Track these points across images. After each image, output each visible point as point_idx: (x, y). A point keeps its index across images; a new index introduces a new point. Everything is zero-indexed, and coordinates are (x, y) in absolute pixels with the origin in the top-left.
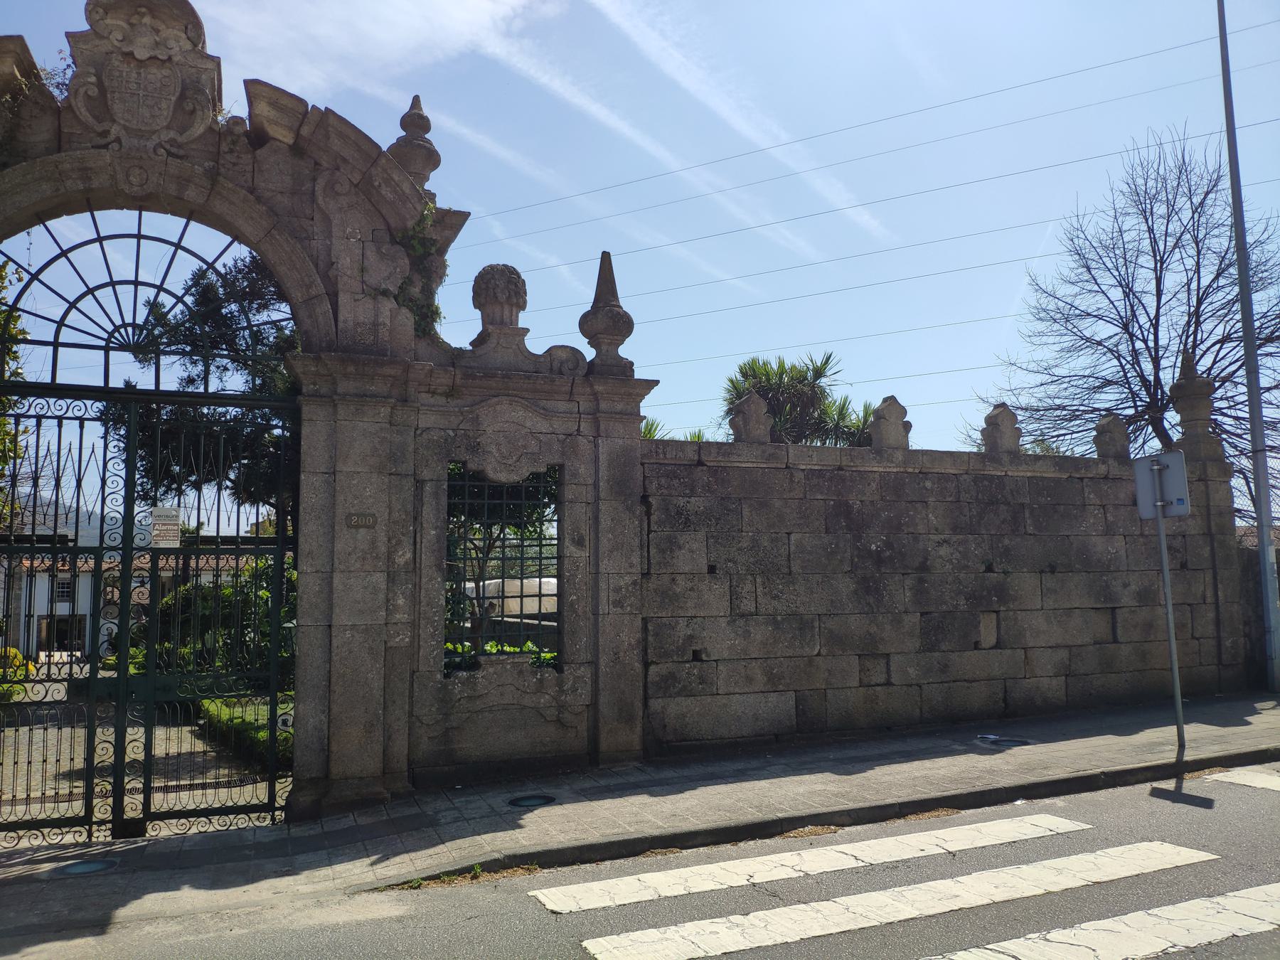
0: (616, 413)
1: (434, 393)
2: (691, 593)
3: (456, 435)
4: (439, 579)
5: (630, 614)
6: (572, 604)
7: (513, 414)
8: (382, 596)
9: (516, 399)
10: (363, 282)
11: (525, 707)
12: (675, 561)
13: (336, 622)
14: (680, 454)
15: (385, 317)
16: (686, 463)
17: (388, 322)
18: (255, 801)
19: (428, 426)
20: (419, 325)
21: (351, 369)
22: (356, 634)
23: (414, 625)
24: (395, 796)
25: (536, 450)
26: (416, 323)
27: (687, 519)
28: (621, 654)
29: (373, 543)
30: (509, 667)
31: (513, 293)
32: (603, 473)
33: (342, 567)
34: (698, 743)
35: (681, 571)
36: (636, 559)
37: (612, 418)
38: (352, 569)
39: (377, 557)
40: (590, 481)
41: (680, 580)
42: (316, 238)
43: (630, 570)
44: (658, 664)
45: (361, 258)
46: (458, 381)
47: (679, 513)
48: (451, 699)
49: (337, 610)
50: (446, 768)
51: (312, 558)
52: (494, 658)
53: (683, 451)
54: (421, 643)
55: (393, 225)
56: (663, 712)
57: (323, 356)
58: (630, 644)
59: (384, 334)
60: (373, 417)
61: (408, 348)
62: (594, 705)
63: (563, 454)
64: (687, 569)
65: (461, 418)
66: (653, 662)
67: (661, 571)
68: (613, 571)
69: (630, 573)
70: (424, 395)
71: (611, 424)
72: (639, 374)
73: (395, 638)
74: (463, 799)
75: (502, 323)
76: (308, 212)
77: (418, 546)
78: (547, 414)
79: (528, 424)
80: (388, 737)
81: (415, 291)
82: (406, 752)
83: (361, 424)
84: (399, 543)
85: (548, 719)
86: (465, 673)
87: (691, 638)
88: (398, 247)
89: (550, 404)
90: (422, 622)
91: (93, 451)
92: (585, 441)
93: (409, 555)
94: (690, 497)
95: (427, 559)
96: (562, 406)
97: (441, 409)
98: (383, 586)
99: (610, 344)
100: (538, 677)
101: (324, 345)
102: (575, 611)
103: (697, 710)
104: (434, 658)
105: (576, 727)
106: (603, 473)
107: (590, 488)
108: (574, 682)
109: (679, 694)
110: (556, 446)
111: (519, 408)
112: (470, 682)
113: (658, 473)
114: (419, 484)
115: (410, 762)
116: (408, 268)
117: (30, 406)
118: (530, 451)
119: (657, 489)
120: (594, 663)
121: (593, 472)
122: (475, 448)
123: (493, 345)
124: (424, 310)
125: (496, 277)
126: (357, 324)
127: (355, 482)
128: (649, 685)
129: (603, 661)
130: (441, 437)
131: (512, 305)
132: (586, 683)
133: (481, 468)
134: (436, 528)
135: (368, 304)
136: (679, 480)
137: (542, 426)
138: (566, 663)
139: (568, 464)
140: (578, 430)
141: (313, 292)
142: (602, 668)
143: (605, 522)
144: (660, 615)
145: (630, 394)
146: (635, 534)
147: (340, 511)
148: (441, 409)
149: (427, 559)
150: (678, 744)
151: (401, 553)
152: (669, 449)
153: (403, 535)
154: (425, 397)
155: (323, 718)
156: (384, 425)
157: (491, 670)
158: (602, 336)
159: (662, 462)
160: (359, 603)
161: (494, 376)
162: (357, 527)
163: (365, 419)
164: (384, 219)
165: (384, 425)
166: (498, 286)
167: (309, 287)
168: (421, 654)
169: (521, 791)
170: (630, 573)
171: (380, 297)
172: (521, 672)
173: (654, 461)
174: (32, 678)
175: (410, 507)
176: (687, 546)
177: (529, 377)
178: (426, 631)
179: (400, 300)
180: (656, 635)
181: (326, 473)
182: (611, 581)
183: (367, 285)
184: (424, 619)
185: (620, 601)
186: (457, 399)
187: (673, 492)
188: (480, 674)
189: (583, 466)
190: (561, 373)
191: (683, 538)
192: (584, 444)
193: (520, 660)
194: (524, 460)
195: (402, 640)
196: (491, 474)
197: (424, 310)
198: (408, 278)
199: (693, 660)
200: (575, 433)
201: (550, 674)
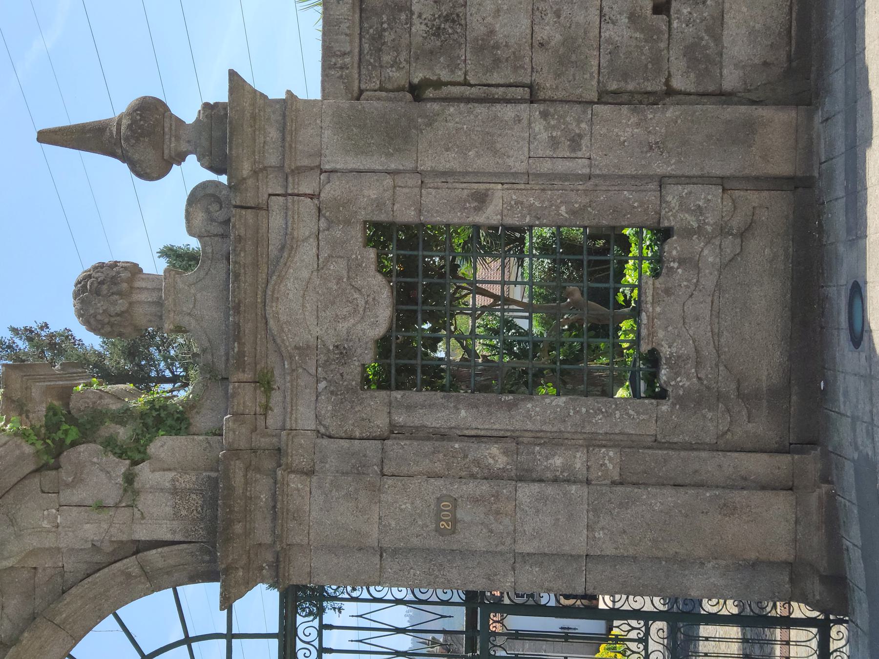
0: (283, 139)
1: (267, 408)
2: (564, 15)
3: (325, 379)
4: (529, 405)
5: (591, 123)
6: (573, 213)
7: (291, 296)
8: (550, 490)
9: (269, 293)
10: (116, 506)
11: (718, 286)
12: (512, 41)
13: (582, 550)
14: (344, 26)
15: (165, 479)
16: (357, 16)
17: (171, 475)
18: (814, 644)
19: (313, 417)
20: (171, 427)
21: (238, 528)
22: (600, 525)
23: (592, 443)
24: (825, 478)
25: (343, 263)
26: (169, 433)
27: (447, 18)
28: (652, 139)
29: (476, 501)
30: (658, 309)
31: (115, 289)
32: (375, 162)
33: (509, 541)
34: (795, 8)
35: (529, 31)
36: (508, 112)
37: (291, 146)
38: (511, 528)
39: (497, 496)
40: (388, 181)
41: (542, 34)
42: (60, 564)
43: (525, 122)
44: (670, 75)
45: (82, 508)
46: (248, 376)
47: (438, 32)
48: (698, 391)
49: (567, 549)
50: (794, 398)
51: (496, 575)
52: (644, 332)
53: (339, 23)
54: (617, 431)
55: (32, 467)
56: (744, 67)
57: (223, 566)
58: (638, 125)
59: (188, 480)
60: (303, 498)
61: (205, 445)
62: (723, 183)
63: (348, 222)
64: (526, 22)
65: (300, 370)
66: (667, 83)
67: (528, 67)
68: (526, 149)
69: (530, 123)
70: (270, 421)
71: (300, 147)
72: (220, 94)
73: (608, 470)
74: (842, 399)
75: (159, 303)
76: (25, 574)
77: (482, 433)
78: (289, 245)
79: (305, 274)
80: (744, 483)
81: (123, 433)
82: (765, 456)
83: (313, 513)
84: (477, 462)
85: (738, 251)
86: (663, 372)
87: (634, 18)
88: (63, 459)
89: (275, 239)
90: (588, 429)
91: (361, 616)
92: (328, 187)
93: (495, 450)
94: (412, 13)
95: (500, 422)
96: (276, 221)
97: (288, 399)
98: (535, 487)
99: (178, 138)
100: (676, 265)
101: (207, 558)
102: (583, 208)
103: (744, 9)
104: (638, 413)
105: (754, 208)
106: (375, 162)
107: (400, 180)
108: (688, 211)
109: (717, 39)
110: (337, 232)
111: (282, 288)
112: (677, 363)
113: (374, 67)
114: (394, 431)
115: (781, 450)
116: (92, 446)
117: (308, 643)
118: (345, 273)
119: (399, 69)
120: (662, 181)
121: (375, 177)
122: (343, 353)
123: (193, 322)
124: (150, 421)
125: (92, 312)
126: (176, 516)
127: (393, 523)
128: (701, 89)
129: (659, 168)
130: (329, 399)
131: (132, 288)
132: (690, 193)
133: (371, 345)
134: (457, 408)
135: (146, 502)
136: (384, 30)
137: (307, 253)
138: (659, 222)
139: (362, 215)
140: (312, 196)
141: (135, 571)
142: (669, 170)
143: (450, 161)
144: (595, 69)
145: (254, 117)
146: (470, 112)
147: (434, 542)
148: (288, 399)
149: (500, 422)
150: (793, 42)
151: (491, 461)
152: (336, 47)
153: (466, 456)
154: (274, 420)
155: (710, 565)
156: (314, 484)
157: (661, 334)
158: (166, 152)
159: (356, 58)
160: (558, 520)
161: (237, 326)
162: (455, 521)
163: (307, 508)
164: (24, 478)
165: (314, 484)
166: (104, 311)
167: (128, 576)
168: (633, 432)
169: (839, 314)
170: (530, 123)
171: (136, 485)
172: (668, 292)
173: (356, 71)
174: (642, 634)
175: (428, 446)
176: (489, 19)
177: (237, 276)
178: (600, 425)
179: (137, 457)
180: (625, 76)
181: (381, 556)
182: (540, 153)
183: (120, 502)
184: (583, 427)
185: (572, 140)
186: (273, 375)
187: (404, 41)
188: (665, 351)
189: (366, 192)
190: (227, 222)
191: (477, 27)
192: (333, 190)
193: (650, 293)
194: (359, 282)
195: (610, 459)
196: (380, 330)
197: (150, 421)
198: (105, 447)
199: (669, 16)
200: (316, 201)
201: (674, 248)
